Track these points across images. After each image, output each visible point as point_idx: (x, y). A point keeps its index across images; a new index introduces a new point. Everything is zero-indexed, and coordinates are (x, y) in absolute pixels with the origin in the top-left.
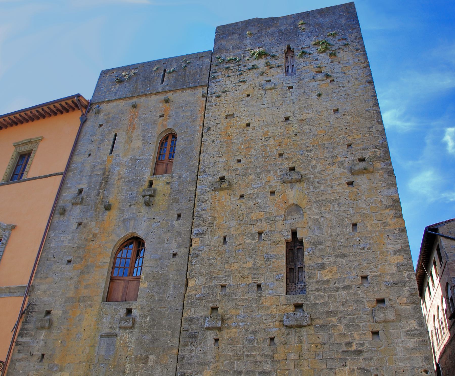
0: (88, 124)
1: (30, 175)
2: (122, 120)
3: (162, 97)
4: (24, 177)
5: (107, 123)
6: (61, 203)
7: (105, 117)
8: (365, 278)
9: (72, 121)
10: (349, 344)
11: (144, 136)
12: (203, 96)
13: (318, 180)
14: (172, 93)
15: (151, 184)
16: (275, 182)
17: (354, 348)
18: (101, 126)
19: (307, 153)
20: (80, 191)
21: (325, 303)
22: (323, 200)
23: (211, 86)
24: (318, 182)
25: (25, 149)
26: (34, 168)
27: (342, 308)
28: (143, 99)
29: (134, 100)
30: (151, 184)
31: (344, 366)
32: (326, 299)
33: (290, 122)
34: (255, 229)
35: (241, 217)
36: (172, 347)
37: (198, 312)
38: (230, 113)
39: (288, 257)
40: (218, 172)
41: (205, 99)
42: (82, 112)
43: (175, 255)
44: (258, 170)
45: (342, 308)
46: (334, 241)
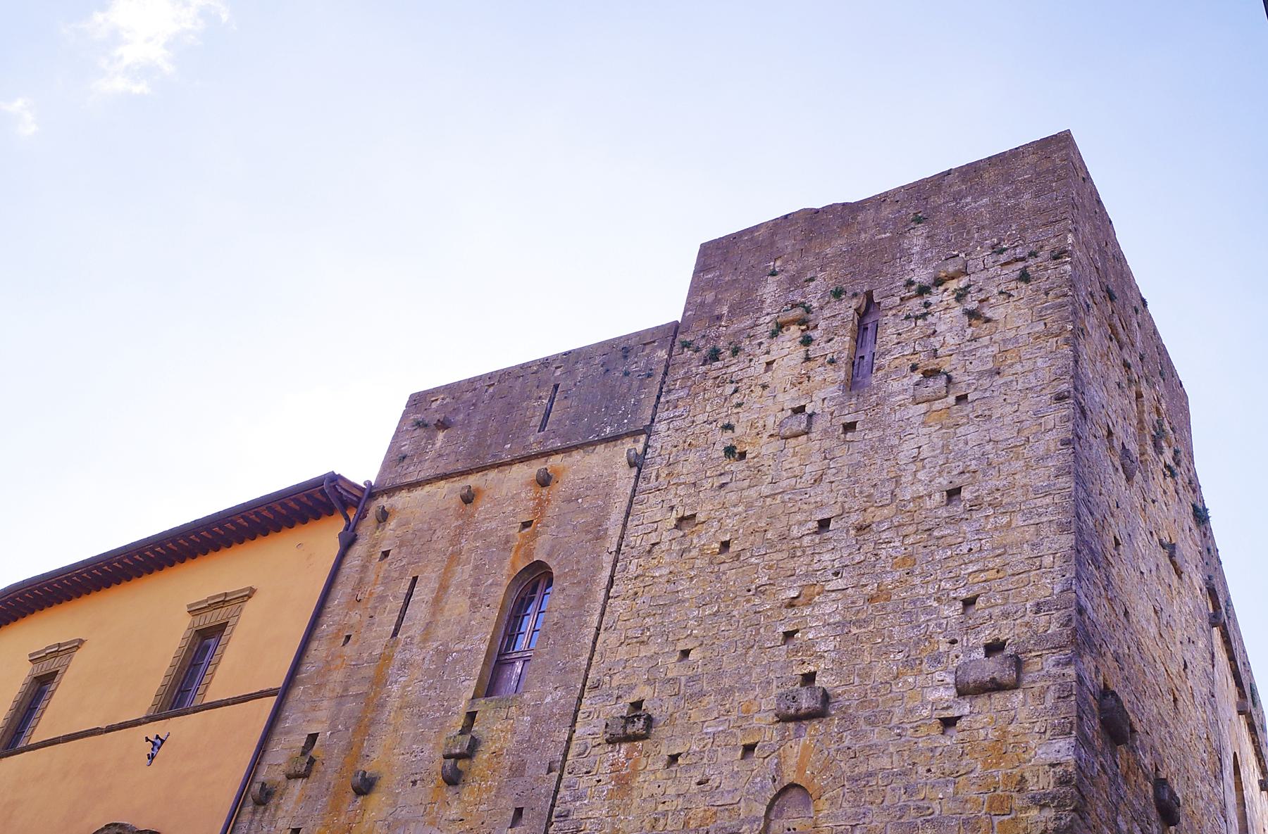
0: (358, 550)
1: (35, 739)
2: (435, 538)
4: (22, 744)
5: (400, 547)
6: (263, 775)
7: (399, 532)
9: (322, 540)
11: (476, 584)
12: (631, 465)
13: (867, 713)
14: (559, 457)
15: (471, 716)
16: (763, 719)
19: (854, 630)
20: (313, 738)
22: (870, 775)
23: (657, 433)
25: (212, 618)
26: (223, 679)
28: (493, 474)
29: (473, 481)
30: (471, 716)
33: (829, 534)
35: (662, 821)
38: (688, 513)
39: (994, 161)
40: (632, 688)
42: (347, 518)
44: (726, 682)
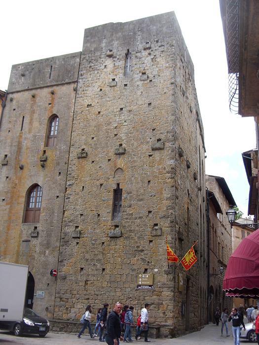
3: (50, 89)
8: (150, 212)
10: (138, 247)
11: (40, 119)
17: (141, 248)
18: (14, 110)
21: (129, 226)
24: (134, 155)
27: (137, 228)
31: (135, 257)
32: (130, 223)
34: (98, 183)
36: (56, 247)
37: (70, 230)
41: (75, 92)
43: (58, 197)
45: (137, 228)
46: (137, 191)
